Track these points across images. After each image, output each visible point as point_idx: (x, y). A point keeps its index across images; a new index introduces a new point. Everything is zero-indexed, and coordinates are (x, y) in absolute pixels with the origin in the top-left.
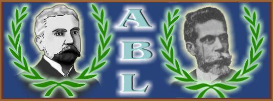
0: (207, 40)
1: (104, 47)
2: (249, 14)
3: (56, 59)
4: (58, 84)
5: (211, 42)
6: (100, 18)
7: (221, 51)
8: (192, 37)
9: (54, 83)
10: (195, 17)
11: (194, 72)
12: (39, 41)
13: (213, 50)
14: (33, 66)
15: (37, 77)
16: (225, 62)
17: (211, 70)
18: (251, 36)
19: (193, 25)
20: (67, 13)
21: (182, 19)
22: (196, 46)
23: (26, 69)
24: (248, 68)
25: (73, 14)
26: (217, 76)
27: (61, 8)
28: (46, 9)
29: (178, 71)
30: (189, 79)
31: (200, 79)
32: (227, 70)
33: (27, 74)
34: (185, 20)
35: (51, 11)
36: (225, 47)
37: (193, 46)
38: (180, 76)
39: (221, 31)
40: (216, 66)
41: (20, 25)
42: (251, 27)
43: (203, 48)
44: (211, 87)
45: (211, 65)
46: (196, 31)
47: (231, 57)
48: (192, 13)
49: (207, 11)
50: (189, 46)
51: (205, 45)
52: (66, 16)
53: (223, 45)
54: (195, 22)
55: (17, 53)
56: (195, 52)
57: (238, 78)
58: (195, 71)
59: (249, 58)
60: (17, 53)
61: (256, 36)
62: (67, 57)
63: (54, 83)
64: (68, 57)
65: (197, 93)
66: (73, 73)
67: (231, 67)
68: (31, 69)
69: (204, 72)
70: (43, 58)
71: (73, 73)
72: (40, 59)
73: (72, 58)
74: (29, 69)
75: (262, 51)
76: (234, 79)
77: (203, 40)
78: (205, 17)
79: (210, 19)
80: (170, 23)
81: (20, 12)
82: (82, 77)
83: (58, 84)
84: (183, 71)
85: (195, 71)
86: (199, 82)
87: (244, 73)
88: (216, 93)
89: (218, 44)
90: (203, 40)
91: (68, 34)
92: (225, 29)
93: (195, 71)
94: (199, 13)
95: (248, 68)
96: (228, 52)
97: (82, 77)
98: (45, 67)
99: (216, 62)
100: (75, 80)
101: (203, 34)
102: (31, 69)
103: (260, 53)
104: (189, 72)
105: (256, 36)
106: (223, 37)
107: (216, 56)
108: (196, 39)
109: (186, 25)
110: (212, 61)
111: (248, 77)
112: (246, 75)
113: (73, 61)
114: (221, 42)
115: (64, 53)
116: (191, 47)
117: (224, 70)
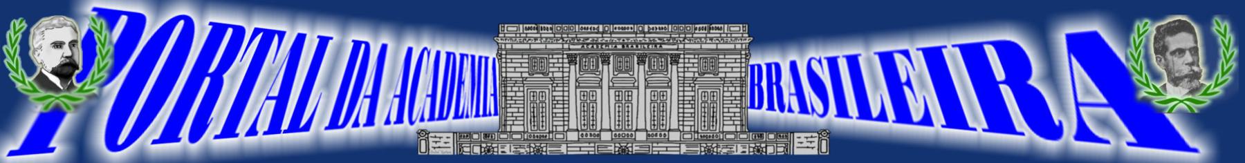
0: (1177, 53)
1: (1227, 63)
2: (1219, 26)
3: (54, 72)
4: (58, 98)
5: (1181, 55)
6: (1223, 32)
7: (1191, 64)
8: (1161, 50)
9: (52, 97)
10: (1165, 29)
11: (1164, 86)
12: (37, 53)
13: (1183, 64)
14: (31, 79)
15: (35, 91)
16: (1195, 76)
17: (1181, 84)
18: (1222, 49)
19: (1164, 37)
20: (65, 25)
21: (1151, 32)
22: (1165, 59)
23: (23, 82)
24: (1218, 82)
25: (72, 26)
26: (1187, 91)
27: (59, 20)
28: (45, 21)
29: (1148, 86)
30: (1159, 93)
31: (1170, 94)
32: (1198, 84)
33: (25, 87)
34: (1155, 32)
35: (50, 24)
36: (1196, 60)
37: (1163, 60)
38: (1150, 91)
39: (1192, 44)
40: (1186, 80)
41: (18, 37)
42: (1222, 40)
43: (1173, 61)
44: (1181, 101)
45: (1181, 79)
46: (1166, 44)
47: (1201, 71)
48: (1162, 26)
49: (1177, 23)
50: (1159, 59)
51: (1175, 59)
52: (64, 28)
53: (1193, 59)
54: (1164, 35)
55: (1139, 69)
56: (1165, 66)
57: (1209, 92)
58: (1165, 85)
59: (1219, 72)
60: (1139, 69)
61: (1227, 48)
62: (65, 71)
63: (52, 97)
64: (67, 70)
65: (1167, 108)
66: (71, 87)
67: (1201, 81)
68: (29, 83)
69: (1174, 86)
70: (41, 73)
71: (71, 87)
72: (37, 73)
73: (71, 71)
74: (27, 82)
75: (1233, 64)
76: (1205, 94)
77: (1173, 53)
78: (1175, 30)
79: (1180, 32)
80: (1139, 36)
81: (18, 25)
82: (81, 90)
83: (58, 98)
84: (1153, 85)
85: (1165, 85)
86: (1169, 97)
87: (1215, 87)
88: (1186, 107)
89: (1188, 57)
90: (1173, 53)
91: (66, 47)
92: (1196, 42)
93: (1165, 85)
94: (1169, 25)
95: (1218, 82)
96: (1198, 66)
97: (81, 90)
98: (43, 81)
99: (1186, 76)
100: (73, 93)
101: (1173, 47)
102: (29, 83)
103: (1231, 67)
104: (1158, 86)
105: (1227, 48)
106: (1194, 51)
107: (1186, 70)
108: (1165, 52)
109: (1155, 38)
110: (1182, 74)
111: (1219, 91)
112: (1217, 89)
113: (71, 75)
114: (1192, 55)
115: (63, 66)
116: (1160, 61)
117: (1195, 84)
